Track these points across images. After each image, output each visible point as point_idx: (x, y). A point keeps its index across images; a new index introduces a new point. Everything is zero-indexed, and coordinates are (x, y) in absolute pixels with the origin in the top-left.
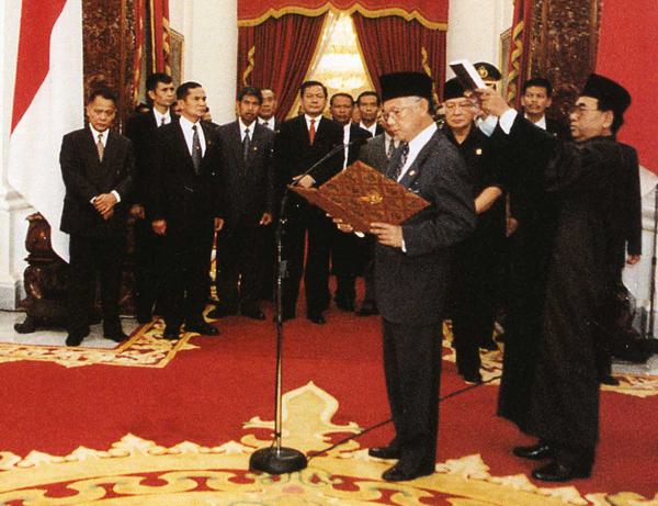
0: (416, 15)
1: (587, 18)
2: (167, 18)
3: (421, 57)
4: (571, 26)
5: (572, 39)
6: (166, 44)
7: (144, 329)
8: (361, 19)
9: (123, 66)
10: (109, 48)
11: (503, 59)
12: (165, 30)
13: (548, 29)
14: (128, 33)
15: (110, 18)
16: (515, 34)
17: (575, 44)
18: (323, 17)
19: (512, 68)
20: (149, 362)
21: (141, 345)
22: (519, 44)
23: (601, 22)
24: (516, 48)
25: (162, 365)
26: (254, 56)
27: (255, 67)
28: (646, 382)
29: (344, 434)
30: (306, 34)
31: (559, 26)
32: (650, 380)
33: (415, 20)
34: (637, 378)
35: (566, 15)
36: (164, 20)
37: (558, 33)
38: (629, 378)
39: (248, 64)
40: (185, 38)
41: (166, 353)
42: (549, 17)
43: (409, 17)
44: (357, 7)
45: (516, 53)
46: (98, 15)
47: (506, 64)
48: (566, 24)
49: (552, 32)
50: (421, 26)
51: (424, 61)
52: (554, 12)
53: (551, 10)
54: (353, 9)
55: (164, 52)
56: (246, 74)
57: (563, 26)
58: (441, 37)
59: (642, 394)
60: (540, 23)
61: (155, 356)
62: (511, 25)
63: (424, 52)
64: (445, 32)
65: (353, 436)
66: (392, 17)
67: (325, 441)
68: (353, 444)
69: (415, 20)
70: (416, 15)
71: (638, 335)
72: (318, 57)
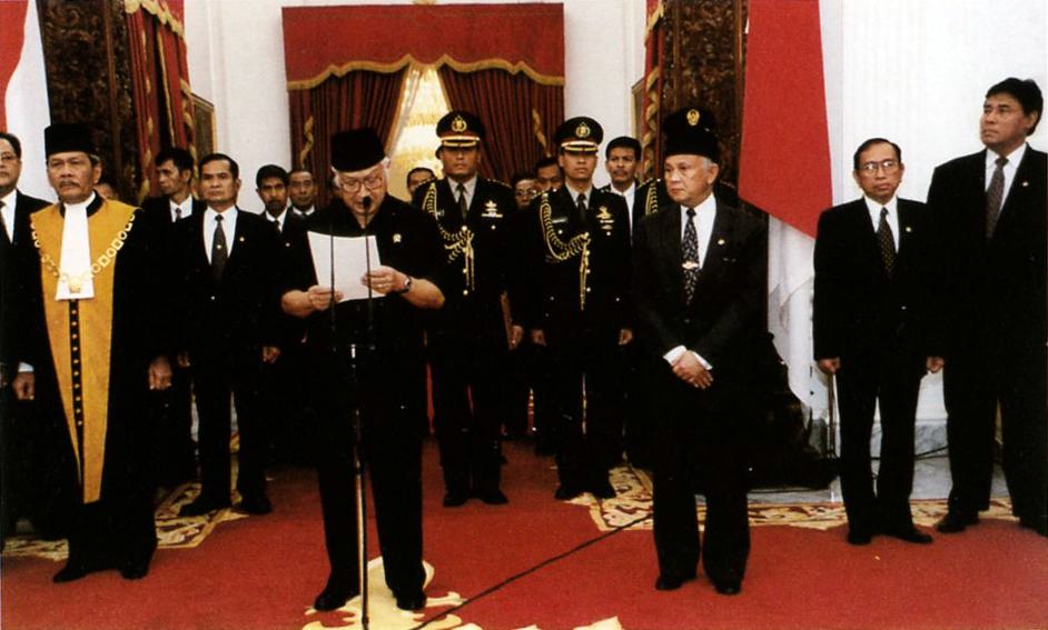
0: (523, 66)
1: (729, 51)
2: (188, 81)
3: (532, 121)
4: (710, 62)
5: (713, 80)
6: (188, 116)
7: (173, 497)
8: (451, 74)
9: (117, 139)
10: (93, 114)
11: (637, 124)
12: (184, 95)
13: (683, 69)
14: (120, 93)
15: (92, 73)
16: (648, 86)
17: (717, 86)
18: (398, 77)
19: (648, 129)
20: (176, 541)
21: (165, 520)
22: (654, 97)
23: (747, 45)
24: (651, 102)
25: (194, 544)
26: (313, 130)
27: (315, 146)
28: (828, 511)
29: (444, 607)
30: (383, 96)
31: (696, 65)
32: (832, 508)
33: (521, 73)
34: (816, 507)
35: (704, 50)
36: (183, 82)
37: (694, 74)
38: (807, 509)
39: (305, 140)
40: (216, 108)
41: (201, 528)
42: (682, 53)
43: (512, 69)
44: (446, 59)
45: (651, 109)
46: (75, 68)
47: (642, 123)
48: (704, 63)
49: (687, 73)
50: (531, 81)
51: (536, 128)
52: (689, 45)
53: (684, 43)
54: (440, 62)
55: (186, 125)
56: (303, 154)
57: (700, 64)
58: (559, 91)
59: (823, 526)
60: (672, 62)
61: (185, 533)
62: (643, 75)
63: (536, 115)
64: (562, 88)
65: (451, 610)
66: (492, 71)
67: (416, 620)
68: (452, 620)
69: (521, 73)
70: (523, 66)
71: (817, 454)
72: (397, 130)
